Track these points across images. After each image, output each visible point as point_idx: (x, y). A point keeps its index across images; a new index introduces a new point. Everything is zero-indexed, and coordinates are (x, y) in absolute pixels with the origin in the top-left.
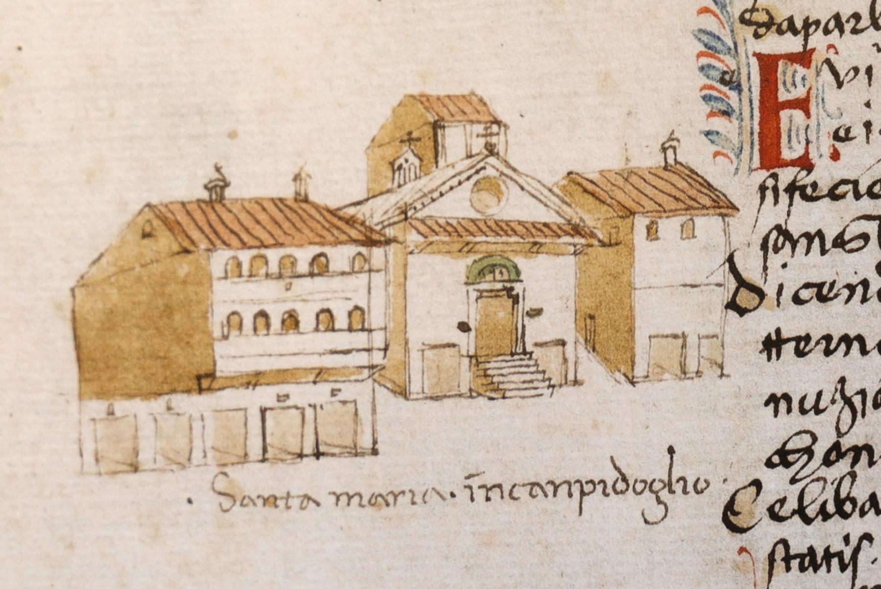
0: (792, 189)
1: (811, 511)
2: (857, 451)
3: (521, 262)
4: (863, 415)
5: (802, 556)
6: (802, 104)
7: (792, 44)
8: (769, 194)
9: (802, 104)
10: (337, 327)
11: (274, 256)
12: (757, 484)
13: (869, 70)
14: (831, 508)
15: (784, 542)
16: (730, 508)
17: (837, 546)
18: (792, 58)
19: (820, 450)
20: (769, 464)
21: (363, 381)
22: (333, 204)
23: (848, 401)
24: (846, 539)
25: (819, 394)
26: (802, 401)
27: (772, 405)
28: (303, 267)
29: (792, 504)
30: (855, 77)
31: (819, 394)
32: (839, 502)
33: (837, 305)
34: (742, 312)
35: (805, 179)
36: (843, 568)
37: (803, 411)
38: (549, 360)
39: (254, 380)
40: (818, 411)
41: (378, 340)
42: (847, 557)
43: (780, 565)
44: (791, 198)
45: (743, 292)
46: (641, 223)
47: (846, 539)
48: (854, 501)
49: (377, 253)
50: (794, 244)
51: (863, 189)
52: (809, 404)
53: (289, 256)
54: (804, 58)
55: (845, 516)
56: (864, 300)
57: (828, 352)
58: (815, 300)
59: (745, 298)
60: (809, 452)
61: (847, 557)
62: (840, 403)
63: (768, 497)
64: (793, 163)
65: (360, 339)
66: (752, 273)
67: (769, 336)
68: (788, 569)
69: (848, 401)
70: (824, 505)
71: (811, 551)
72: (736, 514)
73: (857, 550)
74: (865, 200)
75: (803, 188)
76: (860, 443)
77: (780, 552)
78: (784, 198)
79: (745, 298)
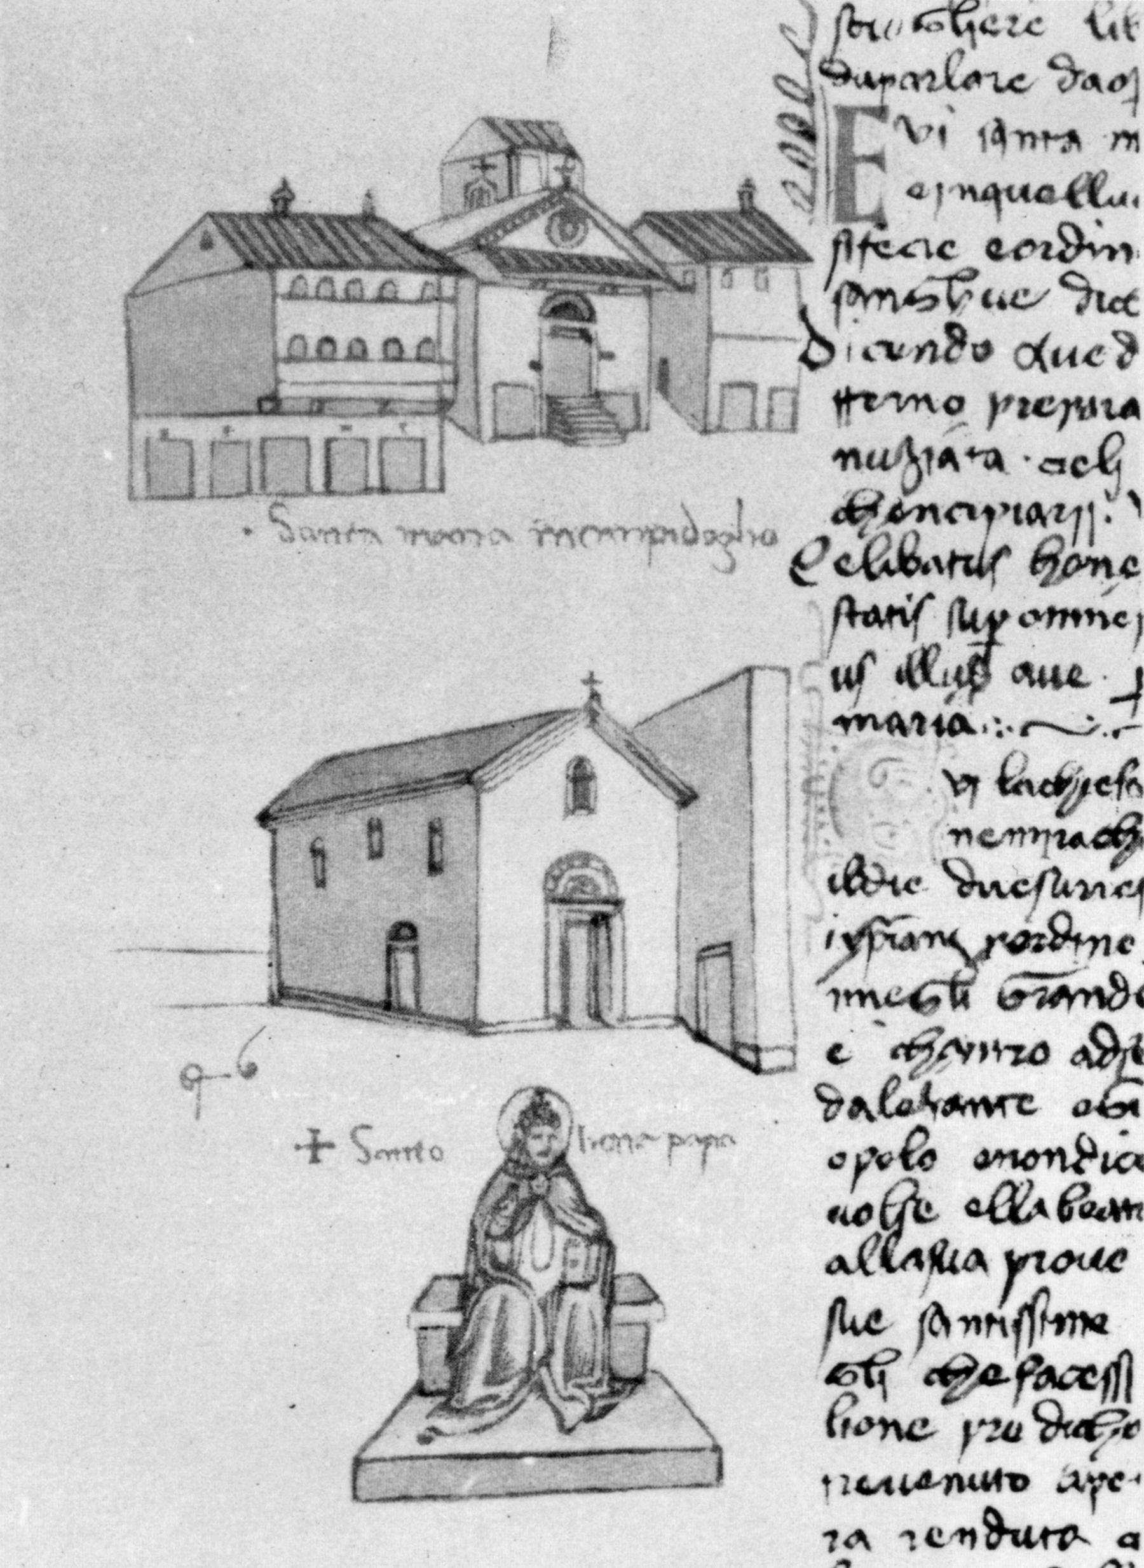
0: (865, 244)
1: (875, 567)
2: (922, 510)
3: (598, 302)
4: (929, 473)
5: (866, 615)
6: (877, 159)
7: (871, 98)
8: (842, 249)
9: (877, 159)
10: (405, 356)
11: (341, 278)
12: (825, 541)
13: (943, 131)
14: (894, 564)
15: (849, 599)
16: (797, 561)
17: (899, 602)
18: (869, 111)
19: (884, 509)
20: (836, 520)
21: (874, 767)
22: (404, 227)
23: (914, 460)
24: (909, 597)
25: (886, 452)
26: (871, 456)
27: (840, 461)
28: (371, 291)
29: (857, 560)
30: (922, 15)
31: (886, 452)
32: (903, 559)
33: (907, 362)
34: (813, 366)
35: (877, 236)
36: (905, 623)
37: (870, 466)
38: (623, 410)
39: (319, 407)
40: (884, 466)
41: (448, 373)
42: (909, 613)
43: (843, 620)
44: (863, 253)
45: (814, 344)
46: (717, 272)
47: (909, 597)
48: (918, 560)
49: (448, 282)
50: (866, 300)
51: (934, 249)
52: (876, 460)
53: (358, 281)
54: (880, 112)
55: (909, 573)
56: (933, 359)
57: (1016, 1062)
58: (1076, 1385)
59: (818, 353)
60: (873, 508)
61: (909, 613)
62: (905, 458)
63: (834, 553)
64: (867, 218)
65: (431, 372)
66: (824, 328)
67: (838, 393)
68: (852, 624)
69: (914, 460)
70: (887, 563)
71: (875, 610)
72: (803, 567)
73: (920, 607)
74: (935, 259)
75: (875, 247)
76: (926, 504)
77: (845, 606)
78: (856, 252)
79: (818, 353)
